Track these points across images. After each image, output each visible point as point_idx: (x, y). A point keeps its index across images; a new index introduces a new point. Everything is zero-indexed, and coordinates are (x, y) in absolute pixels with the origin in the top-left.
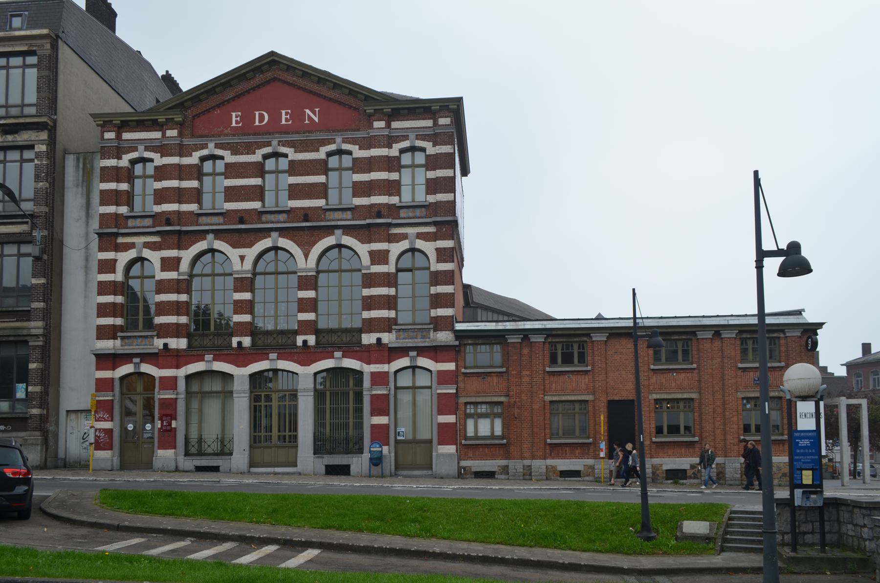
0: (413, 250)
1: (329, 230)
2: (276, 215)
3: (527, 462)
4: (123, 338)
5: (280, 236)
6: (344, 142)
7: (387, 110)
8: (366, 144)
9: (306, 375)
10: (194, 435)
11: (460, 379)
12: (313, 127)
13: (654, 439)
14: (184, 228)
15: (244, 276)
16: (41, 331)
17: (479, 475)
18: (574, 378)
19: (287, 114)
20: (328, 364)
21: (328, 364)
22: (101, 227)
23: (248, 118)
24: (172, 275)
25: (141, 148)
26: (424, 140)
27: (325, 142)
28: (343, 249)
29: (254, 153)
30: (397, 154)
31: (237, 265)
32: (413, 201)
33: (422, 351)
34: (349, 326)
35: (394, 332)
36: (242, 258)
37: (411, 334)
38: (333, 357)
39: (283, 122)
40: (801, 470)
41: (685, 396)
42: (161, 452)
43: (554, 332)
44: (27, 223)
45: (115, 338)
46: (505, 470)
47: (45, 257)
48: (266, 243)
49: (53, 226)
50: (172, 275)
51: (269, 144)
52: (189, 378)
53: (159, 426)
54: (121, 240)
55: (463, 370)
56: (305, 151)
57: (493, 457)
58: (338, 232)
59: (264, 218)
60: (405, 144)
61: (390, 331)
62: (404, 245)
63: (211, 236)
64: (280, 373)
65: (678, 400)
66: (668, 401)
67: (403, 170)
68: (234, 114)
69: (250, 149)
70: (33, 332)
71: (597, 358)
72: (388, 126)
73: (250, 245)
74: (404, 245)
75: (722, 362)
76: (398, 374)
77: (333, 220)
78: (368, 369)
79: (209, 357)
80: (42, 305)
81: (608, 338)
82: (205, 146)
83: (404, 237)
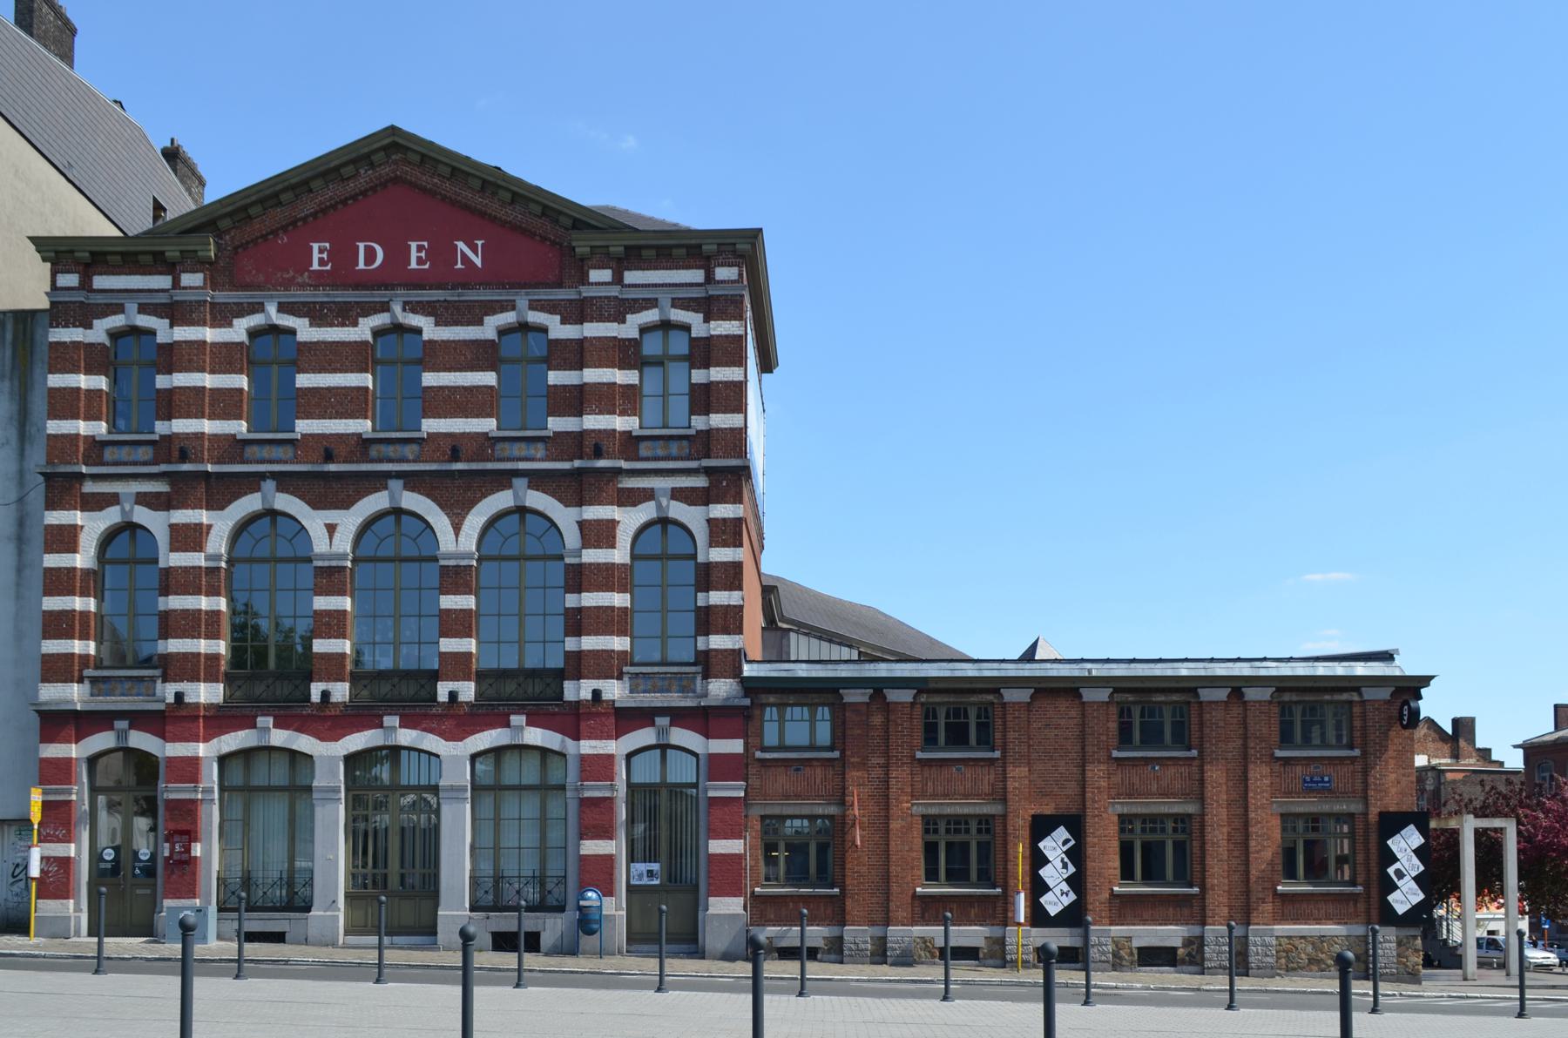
0: (664, 522)
1: (502, 480)
2: (398, 447)
5: (407, 487)
6: (531, 308)
8: (577, 312)
9: (332, 759)
11: (752, 771)
12: (470, 278)
18: (968, 772)
19: (420, 249)
23: (342, 255)
25: (132, 307)
26: (686, 308)
29: (355, 324)
30: (635, 334)
31: (320, 544)
33: (139, 720)
35: (626, 678)
36: (331, 529)
37: (660, 684)
39: (414, 265)
43: (932, 685)
52: (223, 760)
53: (167, 854)
56: (456, 323)
60: (651, 316)
61: (620, 677)
63: (269, 485)
64: (404, 753)
69: (347, 315)
71: (1011, 735)
72: (618, 280)
73: (346, 504)
75: (1245, 746)
76: (635, 760)
82: (258, 308)
83: (648, 495)
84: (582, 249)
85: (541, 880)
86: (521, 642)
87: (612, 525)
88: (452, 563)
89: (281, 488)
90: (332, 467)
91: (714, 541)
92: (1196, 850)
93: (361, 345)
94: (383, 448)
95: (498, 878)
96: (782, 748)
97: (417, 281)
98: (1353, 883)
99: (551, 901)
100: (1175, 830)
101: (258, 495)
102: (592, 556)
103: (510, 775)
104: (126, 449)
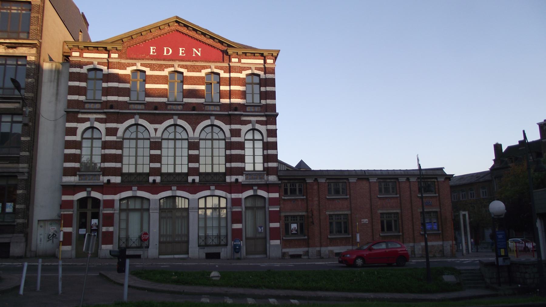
0: (92, 128)
1: (207, 116)
2: (176, 106)
3: (318, 249)
4: (80, 176)
7: (240, 52)
8: (230, 70)
9: (194, 199)
10: (123, 234)
11: (281, 202)
12: (197, 59)
13: (381, 234)
14: (121, 111)
15: (157, 140)
16: (26, 170)
17: (293, 256)
19: (182, 50)
20: (128, 194)
21: (128, 194)
22: (68, 108)
23: (160, 51)
24: (113, 138)
27: (204, 67)
28: (214, 127)
30: (245, 77)
31: (153, 134)
32: (253, 103)
34: (180, 172)
35: (244, 175)
36: (156, 130)
38: (131, 190)
39: (181, 54)
40: (500, 249)
41: (395, 211)
42: (104, 247)
44: (19, 103)
45: (75, 175)
46: (307, 253)
47: (30, 124)
48: (131, 121)
49: (36, 105)
50: (113, 138)
51: (173, 66)
52: (121, 200)
54: (80, 116)
55: (283, 198)
57: (300, 246)
58: (213, 118)
59: (169, 107)
61: (242, 175)
62: (250, 126)
63: (137, 117)
64: (177, 198)
65: (391, 213)
66: (386, 213)
67: (89, 81)
68: (152, 48)
69: (161, 68)
70: (21, 170)
71: (352, 191)
72: (240, 61)
73: (161, 123)
74: (250, 126)
75: (411, 193)
76: (200, 200)
77: (209, 111)
78: (117, 197)
79: (135, 188)
80: (27, 154)
81: (357, 180)
83: (88, 120)
84: (230, 51)
85: (219, 237)
86: (136, 164)
87: (240, 130)
88: (192, 141)
89: (180, 118)
90: (157, 112)
91: (107, 135)
92: (400, 223)
93: (166, 77)
94: (171, 106)
95: (206, 237)
96: (220, 197)
97: (182, 59)
98: (438, 230)
99: (222, 243)
100: (300, 220)
101: (133, 119)
102: (234, 139)
103: (131, 206)
104: (92, 105)
